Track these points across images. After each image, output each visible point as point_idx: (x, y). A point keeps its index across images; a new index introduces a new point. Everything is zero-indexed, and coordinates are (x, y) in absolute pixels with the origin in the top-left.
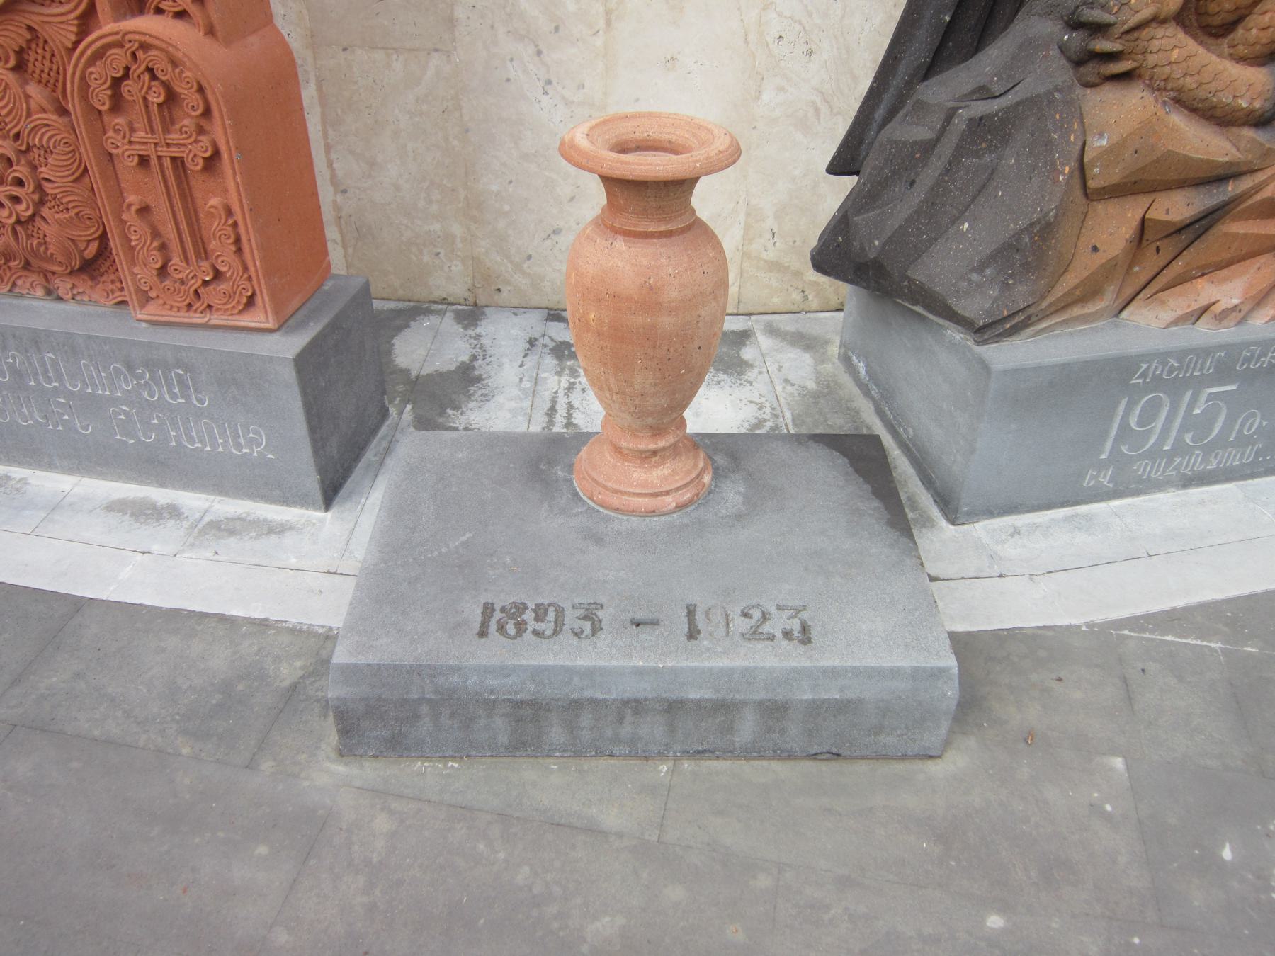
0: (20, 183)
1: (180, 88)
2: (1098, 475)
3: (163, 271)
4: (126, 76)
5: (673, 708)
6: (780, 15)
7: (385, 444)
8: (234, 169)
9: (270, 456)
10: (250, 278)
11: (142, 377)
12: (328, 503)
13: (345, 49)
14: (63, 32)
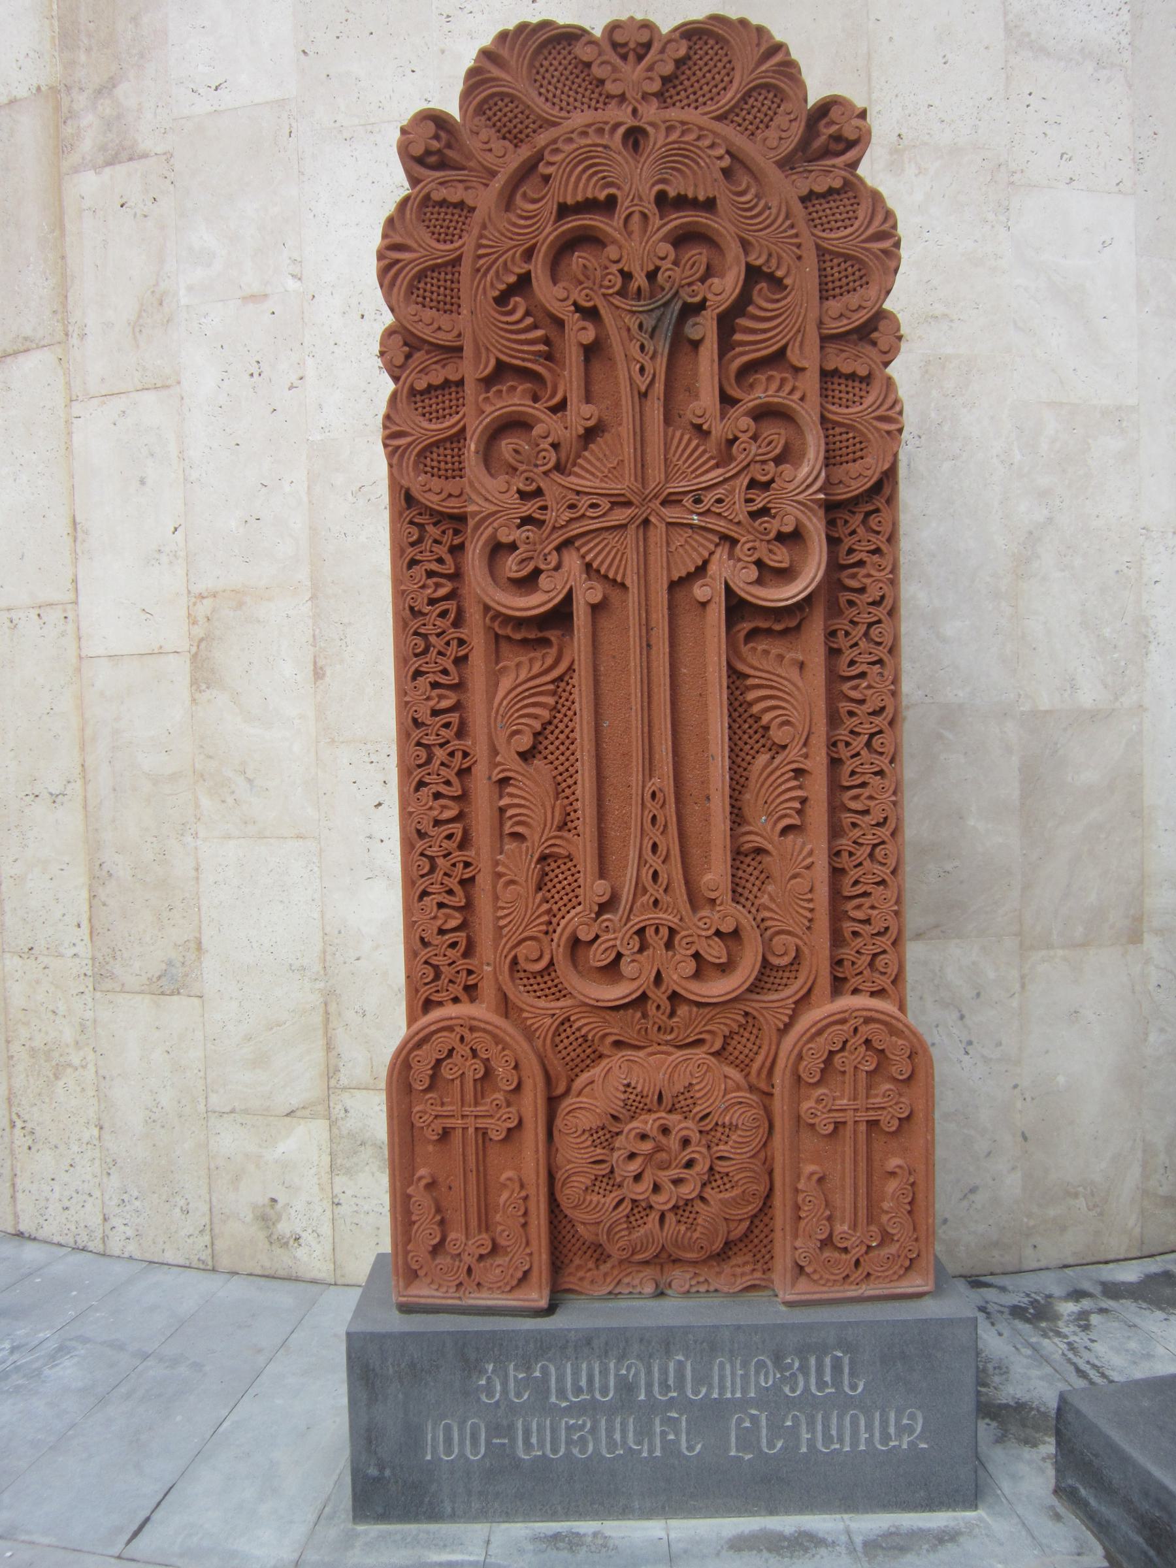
4: (843, 1049)
6: (1157, 967)
11: (790, 1366)
14: (778, 1016)
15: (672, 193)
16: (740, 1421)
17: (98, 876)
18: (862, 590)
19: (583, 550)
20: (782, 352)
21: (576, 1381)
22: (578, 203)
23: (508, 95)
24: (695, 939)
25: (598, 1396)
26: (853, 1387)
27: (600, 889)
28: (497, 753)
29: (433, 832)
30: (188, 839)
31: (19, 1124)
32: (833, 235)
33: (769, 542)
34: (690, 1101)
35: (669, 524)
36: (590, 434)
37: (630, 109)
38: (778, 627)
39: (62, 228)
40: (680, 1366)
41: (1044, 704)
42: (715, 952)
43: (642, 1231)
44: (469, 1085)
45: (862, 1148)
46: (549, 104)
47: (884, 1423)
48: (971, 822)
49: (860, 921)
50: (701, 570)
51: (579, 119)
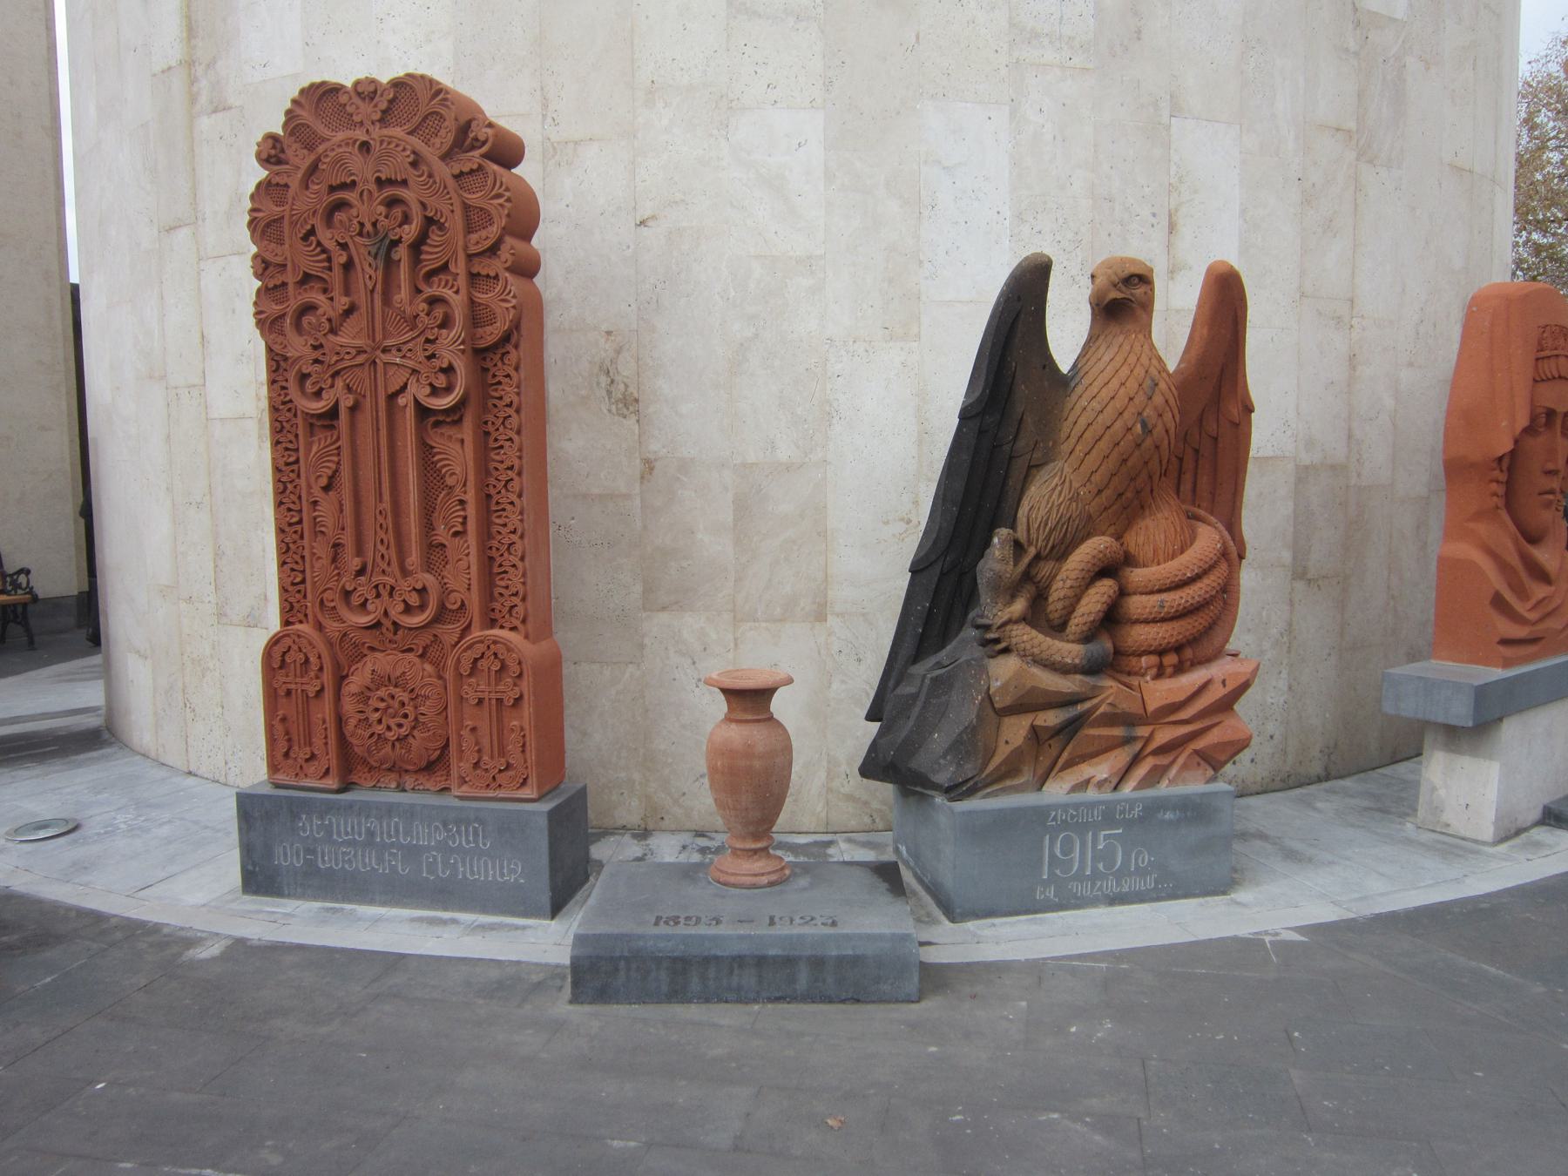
0: (406, 716)
1: (509, 662)
2: (1045, 891)
3: (476, 765)
4: (482, 657)
5: (761, 961)
6: (839, 638)
7: (587, 893)
8: (529, 704)
9: (522, 881)
10: (527, 768)
11: (452, 830)
12: (553, 918)
13: (575, 663)
15: (384, 178)
16: (428, 858)
17: (218, 554)
18: (501, 398)
19: (345, 377)
20: (446, 264)
21: (346, 828)
22: (338, 185)
23: (306, 124)
24: (403, 592)
25: (357, 837)
26: (485, 845)
27: (356, 563)
28: (311, 488)
29: (287, 529)
30: (259, 532)
31: (188, 705)
32: (474, 196)
33: (435, 373)
34: (405, 681)
35: (385, 363)
36: (349, 312)
37: (365, 130)
38: (448, 420)
39: (193, 151)
40: (397, 826)
41: (751, 458)
42: (414, 600)
43: (383, 751)
44: (298, 665)
45: (494, 714)
46: (327, 128)
47: (502, 868)
48: (699, 536)
49: (503, 587)
50: (404, 388)
51: (341, 136)
